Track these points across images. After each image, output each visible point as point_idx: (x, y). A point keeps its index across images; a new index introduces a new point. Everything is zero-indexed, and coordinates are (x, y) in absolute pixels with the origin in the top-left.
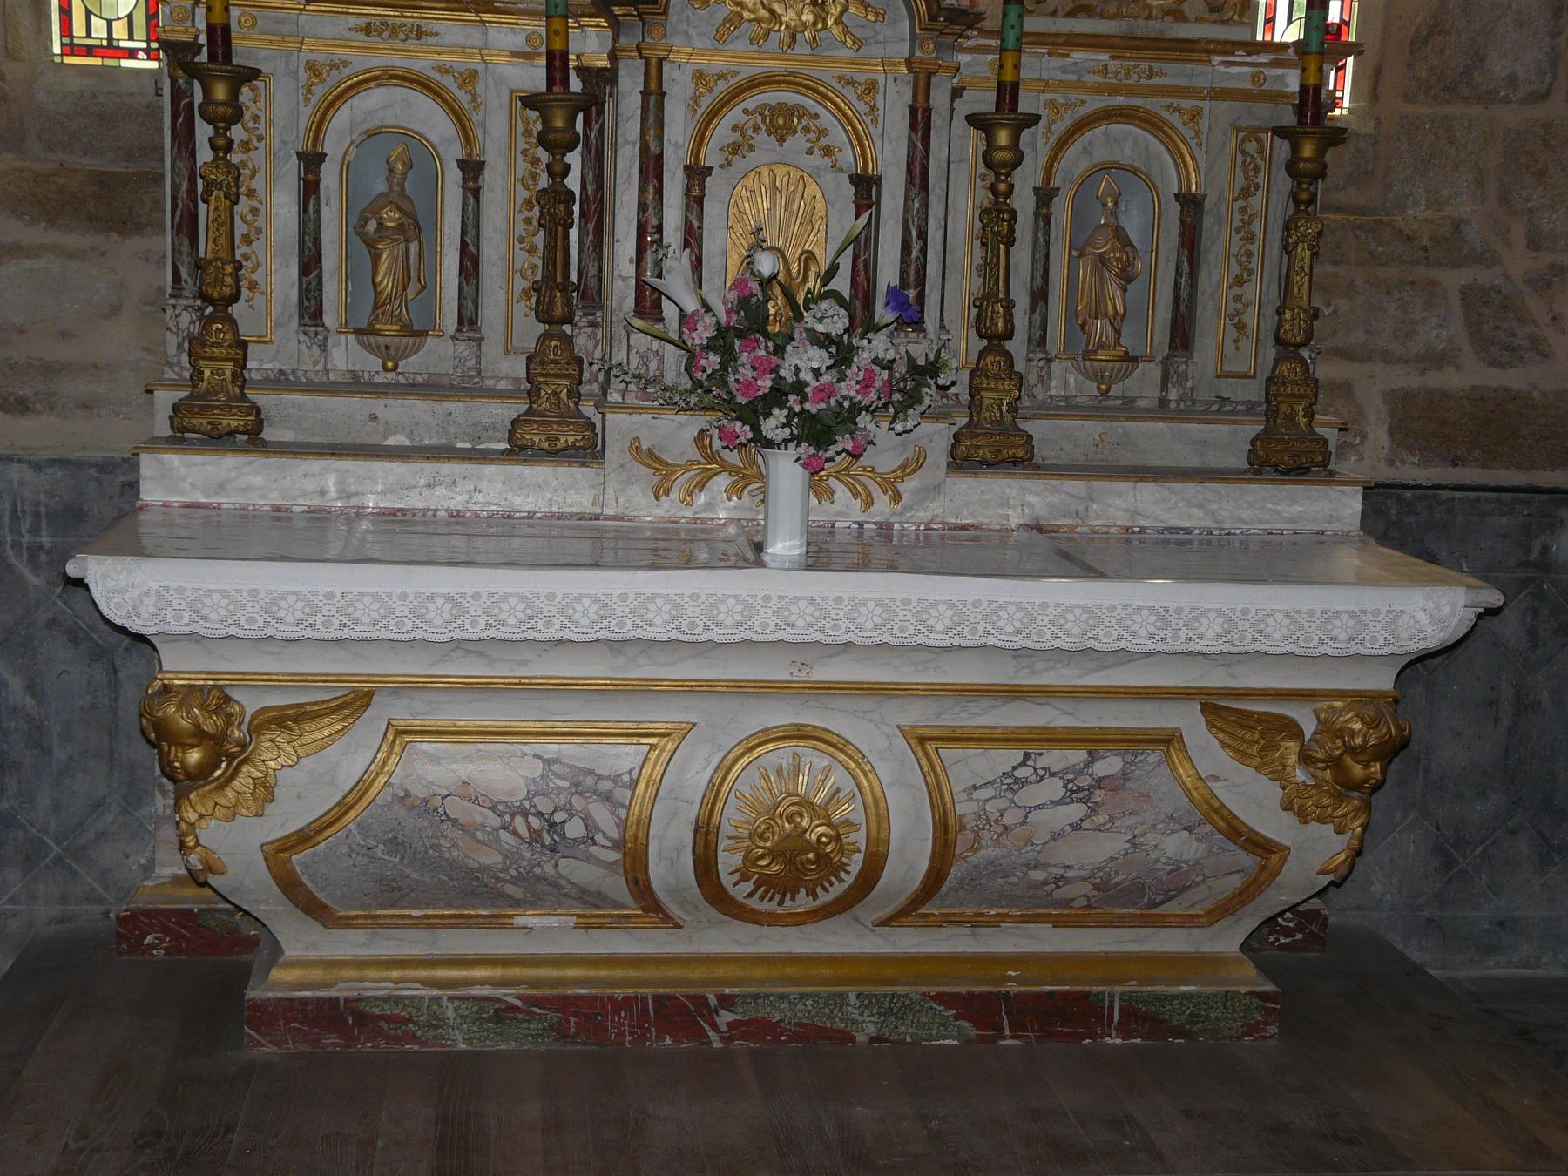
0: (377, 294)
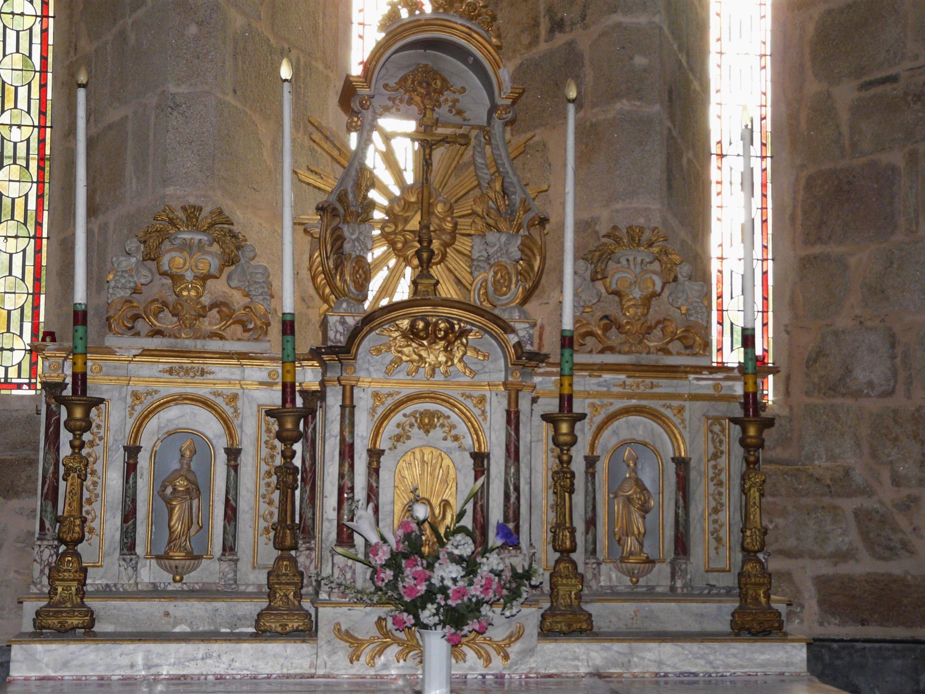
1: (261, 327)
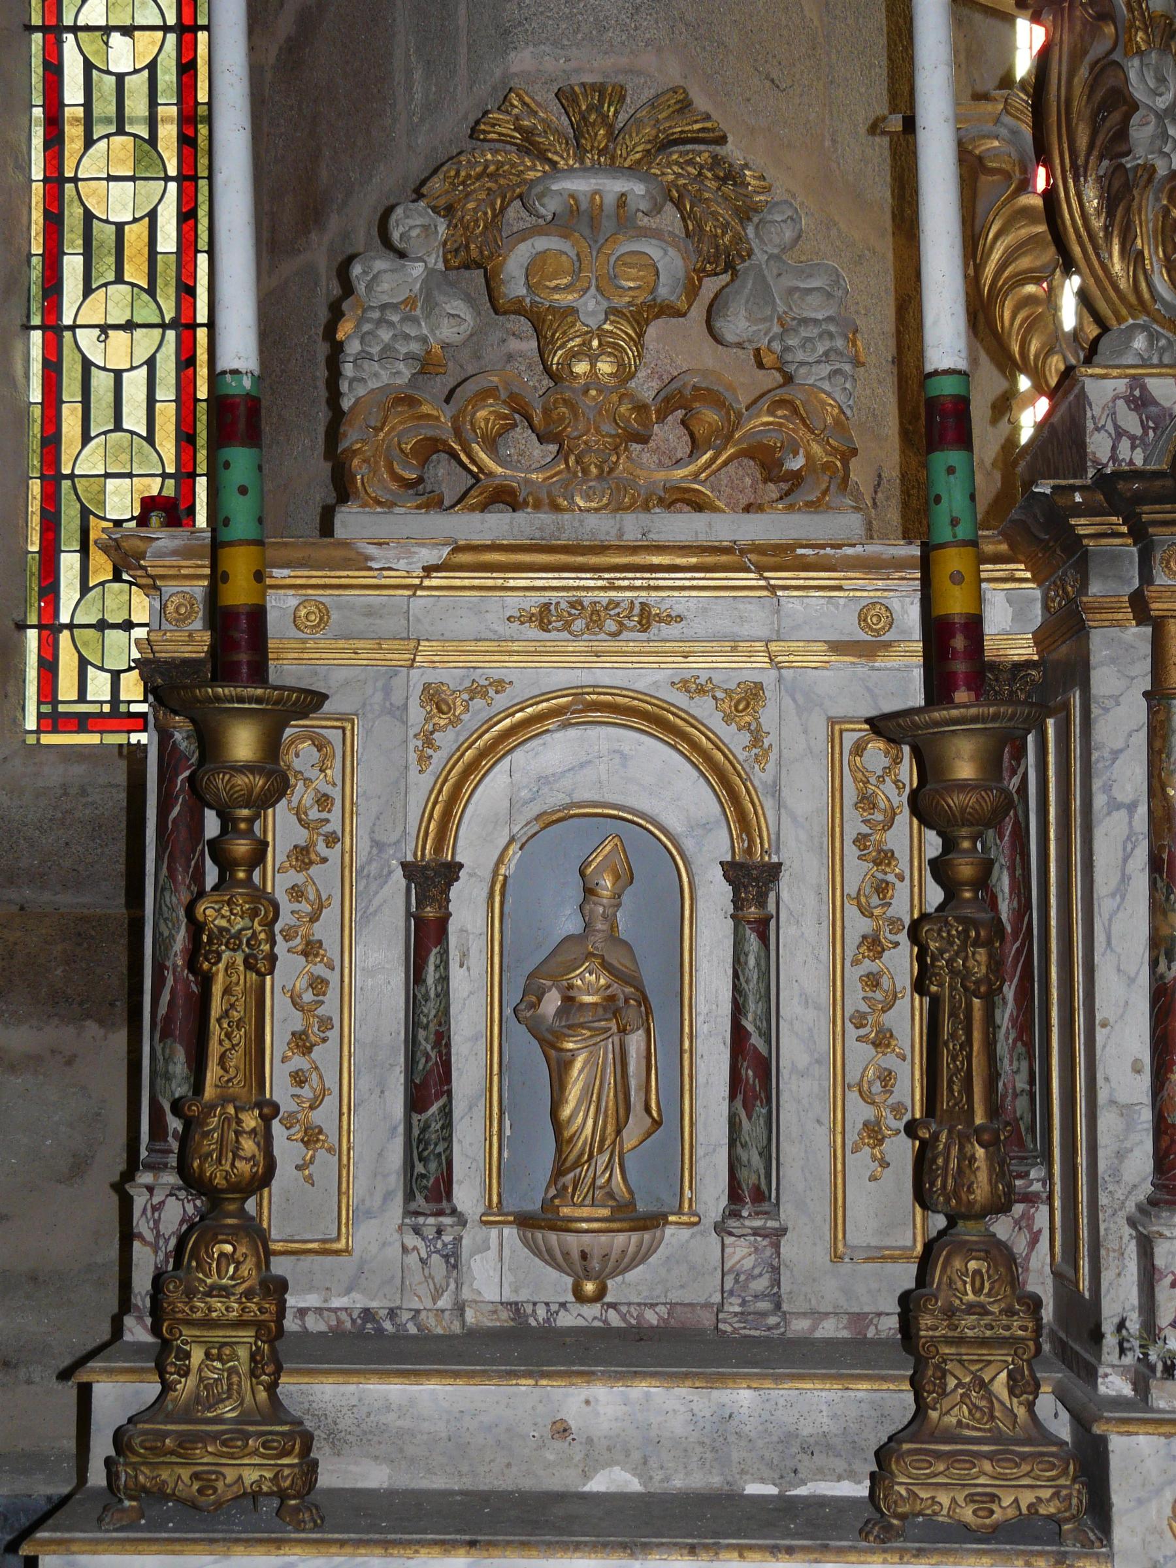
0: (562, 1141)
1: (827, 466)
